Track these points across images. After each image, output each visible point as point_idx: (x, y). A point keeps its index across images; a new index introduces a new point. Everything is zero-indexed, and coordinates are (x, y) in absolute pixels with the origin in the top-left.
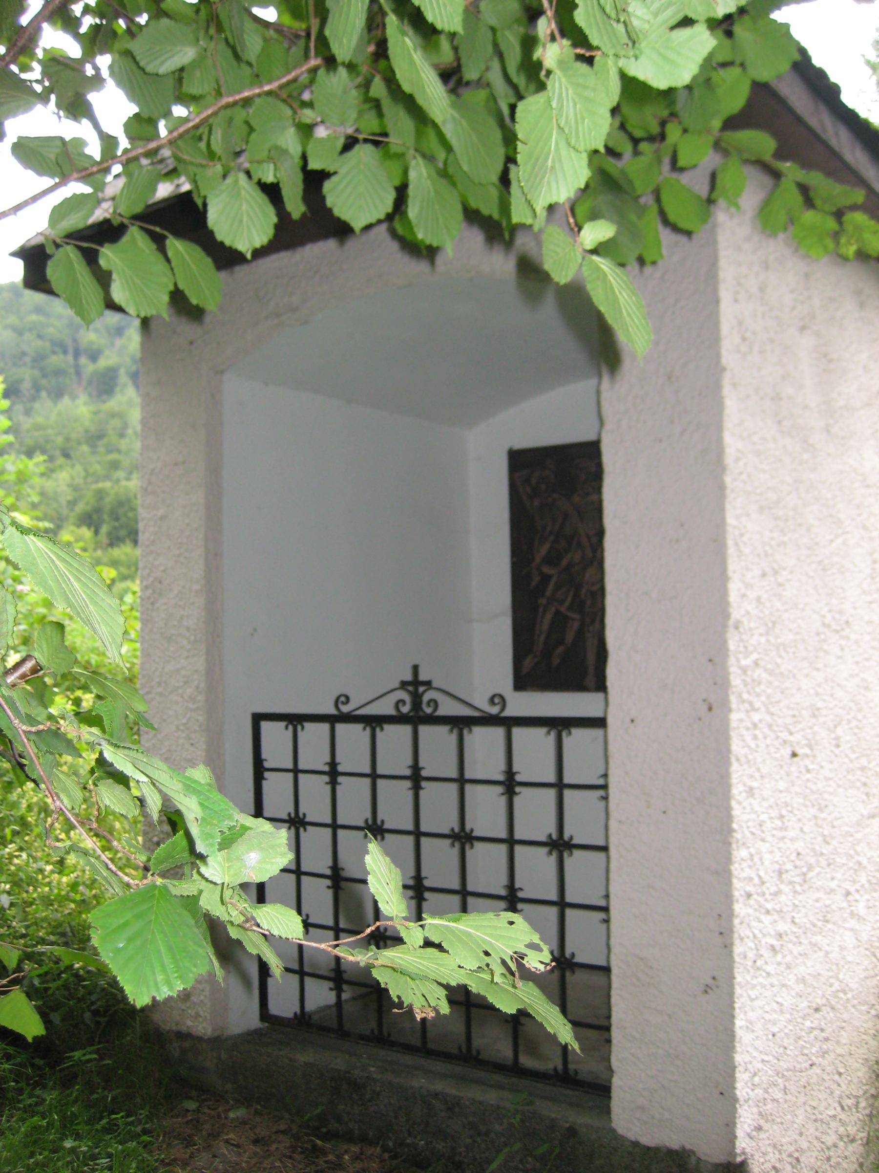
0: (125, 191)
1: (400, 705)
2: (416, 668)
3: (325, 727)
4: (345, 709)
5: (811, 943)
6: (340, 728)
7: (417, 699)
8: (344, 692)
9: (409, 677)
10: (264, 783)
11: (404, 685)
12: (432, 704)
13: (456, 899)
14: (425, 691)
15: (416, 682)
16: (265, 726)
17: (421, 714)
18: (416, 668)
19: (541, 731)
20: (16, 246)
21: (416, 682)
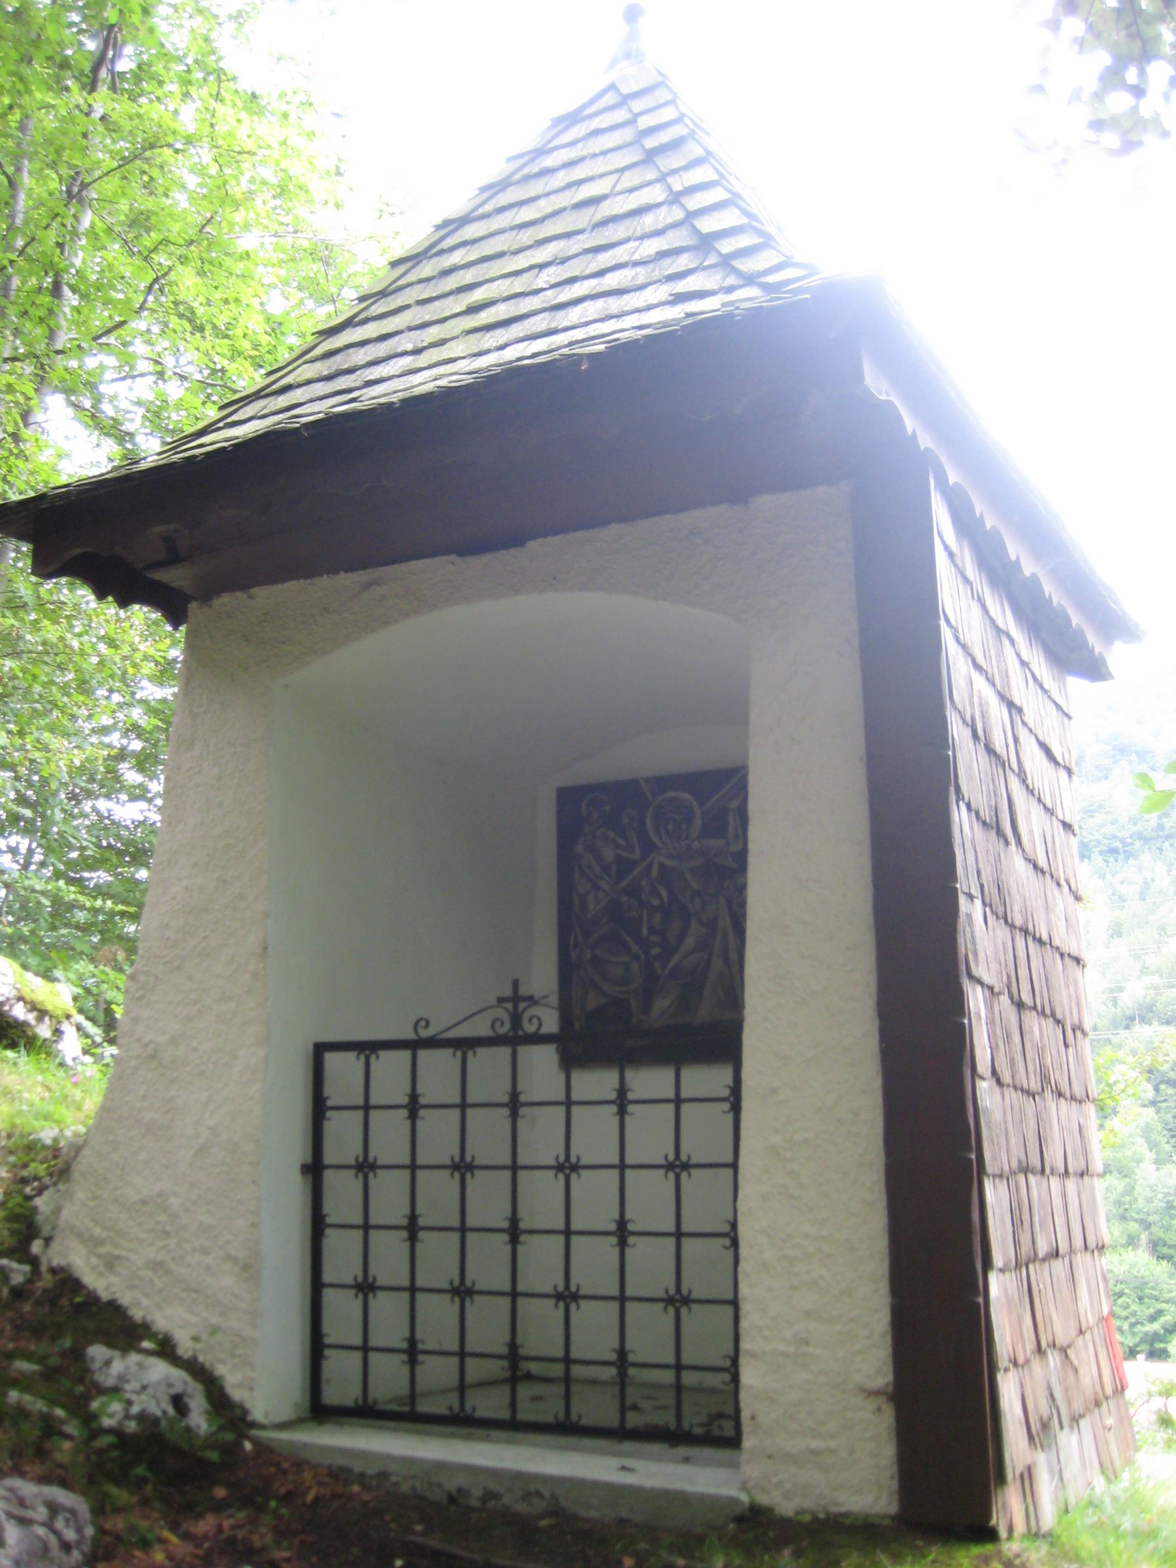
1: (498, 1024)
2: (516, 984)
3: (405, 1056)
4: (425, 1034)
6: (422, 1054)
7: (516, 1019)
8: (425, 1016)
10: (326, 1123)
11: (501, 1000)
12: (535, 1021)
14: (525, 1009)
15: (516, 999)
16: (331, 1059)
17: (521, 1033)
18: (516, 984)
20: (1110, 682)
21: (516, 999)
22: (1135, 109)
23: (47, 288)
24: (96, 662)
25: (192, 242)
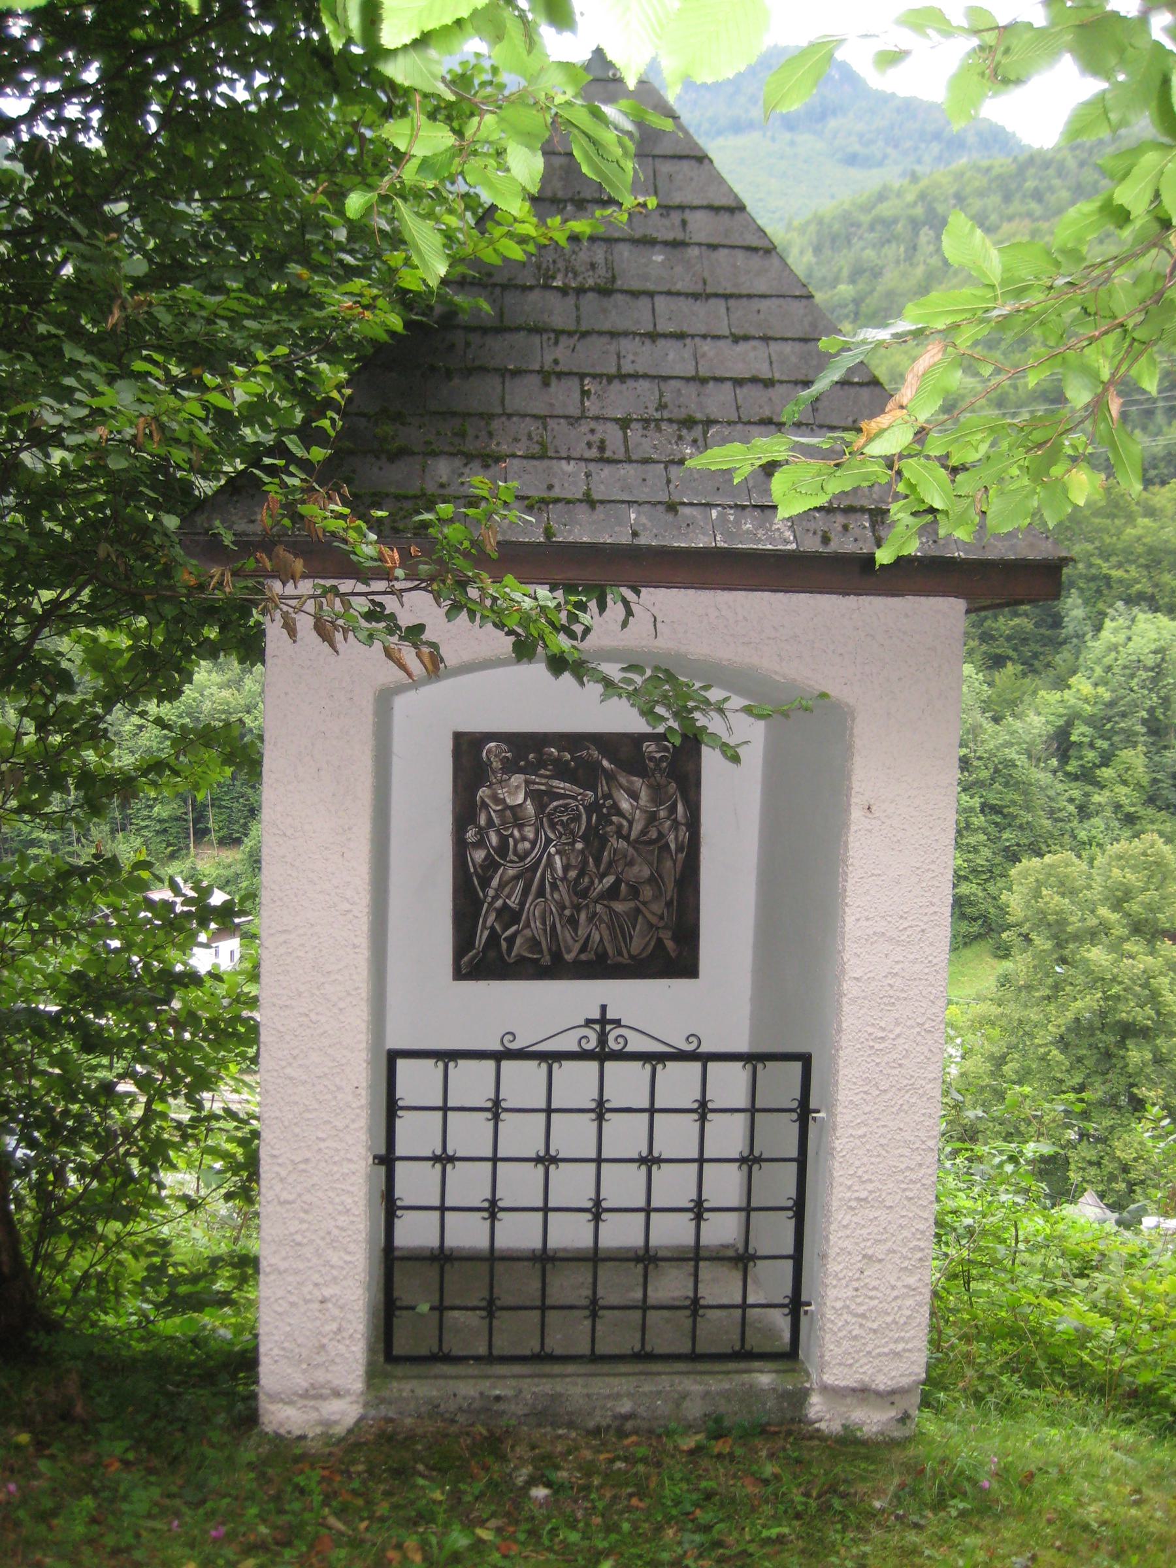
0: (667, 125)
1: (584, 1041)
2: (604, 1008)
3: (490, 1064)
5: (589, 1432)
6: (505, 1064)
7: (603, 1039)
9: (596, 1015)
11: (589, 1022)
13: (703, 1253)
15: (603, 1021)
18: (604, 1008)
19: (398, 1223)
20: (567, 35)
21: (603, 1021)
22: (1096, 182)
23: (1123, 62)
24: (187, 153)
25: (1075, 837)
